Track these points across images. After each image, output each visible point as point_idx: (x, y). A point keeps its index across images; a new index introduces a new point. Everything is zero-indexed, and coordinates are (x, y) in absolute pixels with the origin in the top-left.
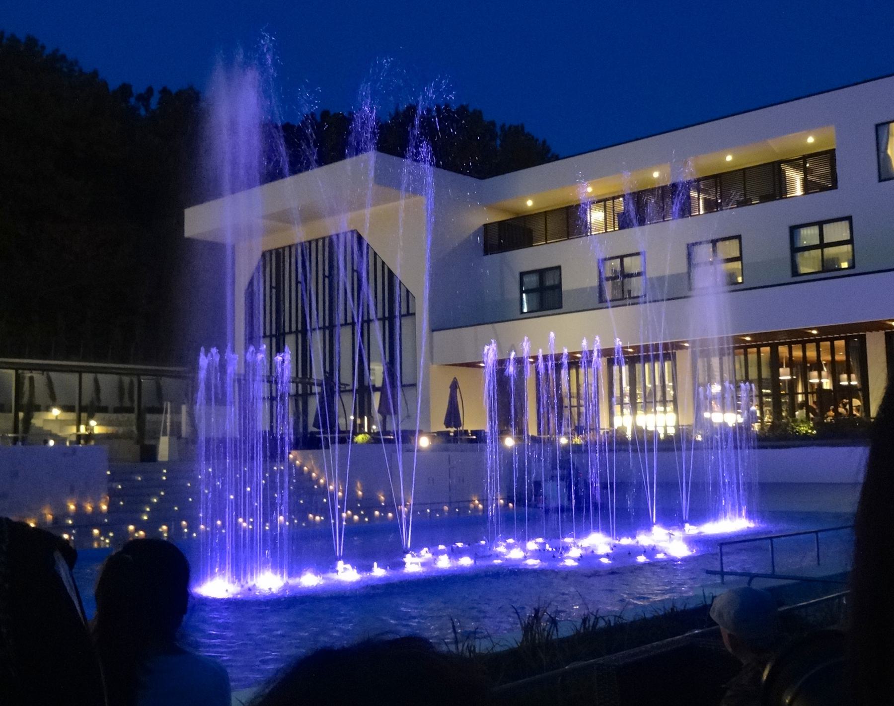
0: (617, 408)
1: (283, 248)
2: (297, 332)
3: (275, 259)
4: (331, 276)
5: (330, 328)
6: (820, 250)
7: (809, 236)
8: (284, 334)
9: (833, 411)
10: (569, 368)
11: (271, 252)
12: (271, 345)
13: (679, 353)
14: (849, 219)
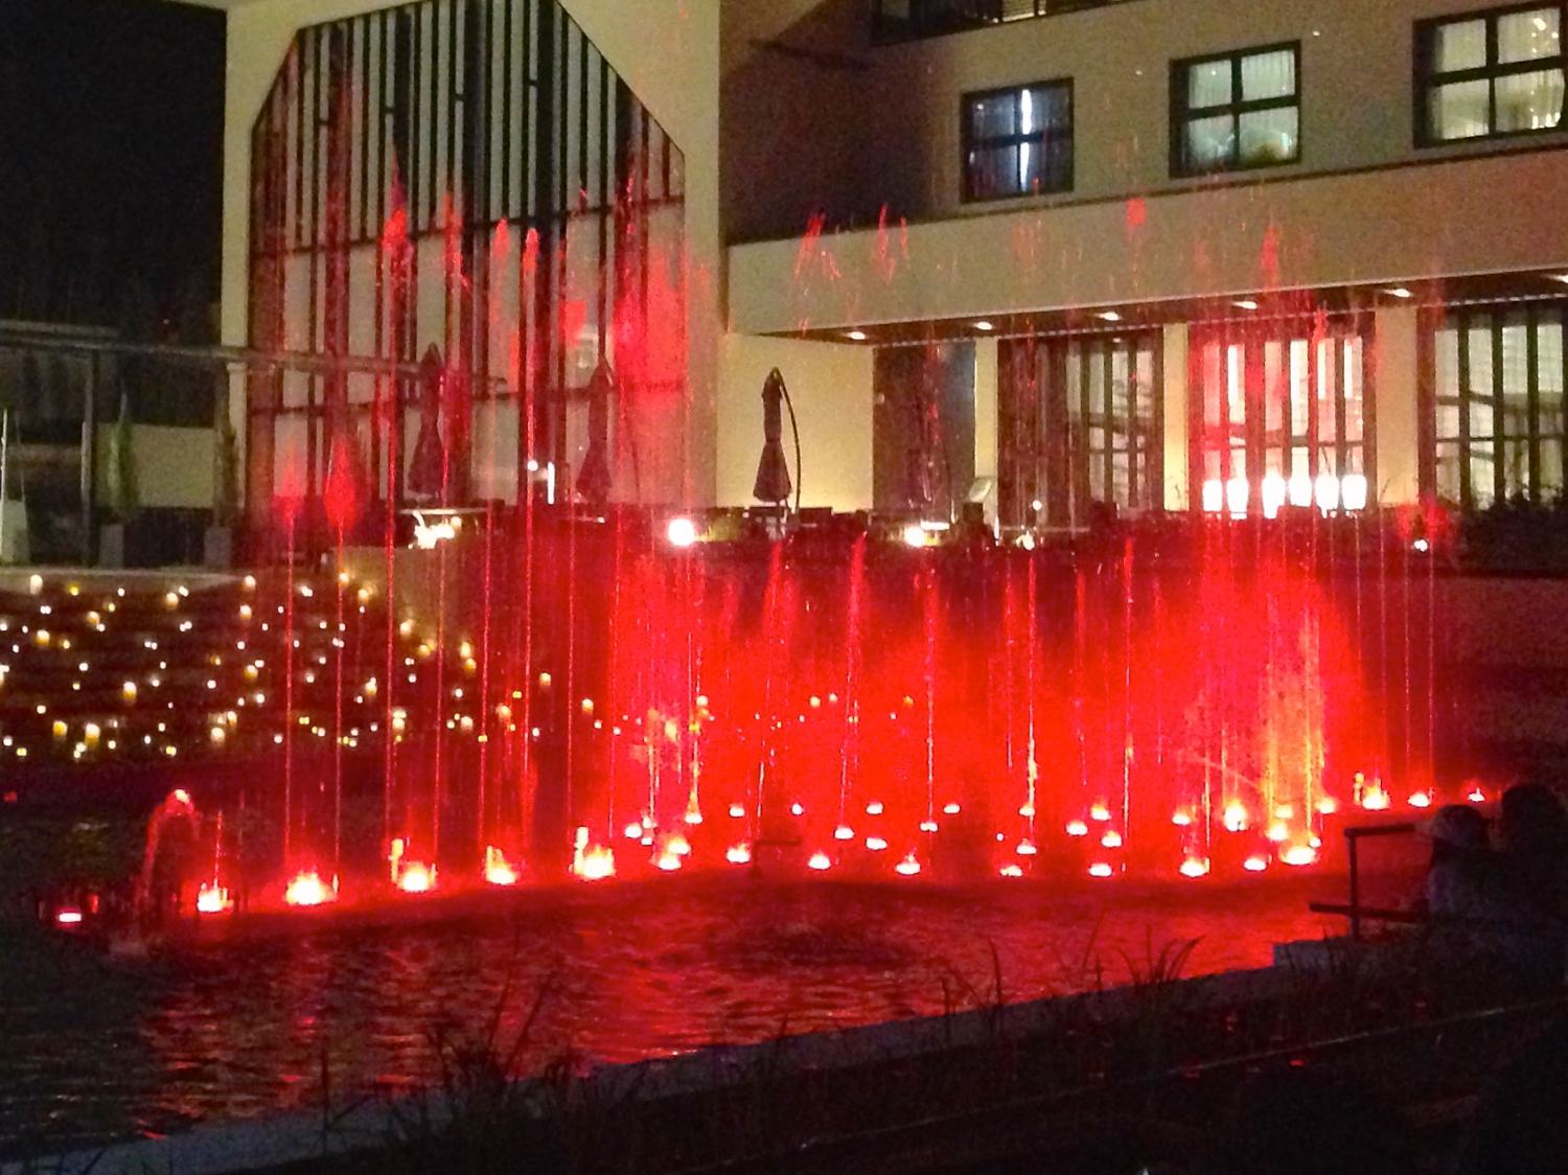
0: (1213, 460)
1: (350, 21)
4: (544, 82)
6: (1487, 82)
7: (1211, 83)
8: (564, 217)
11: (318, 28)
12: (314, 271)
13: (1382, 315)
14: (1295, 46)
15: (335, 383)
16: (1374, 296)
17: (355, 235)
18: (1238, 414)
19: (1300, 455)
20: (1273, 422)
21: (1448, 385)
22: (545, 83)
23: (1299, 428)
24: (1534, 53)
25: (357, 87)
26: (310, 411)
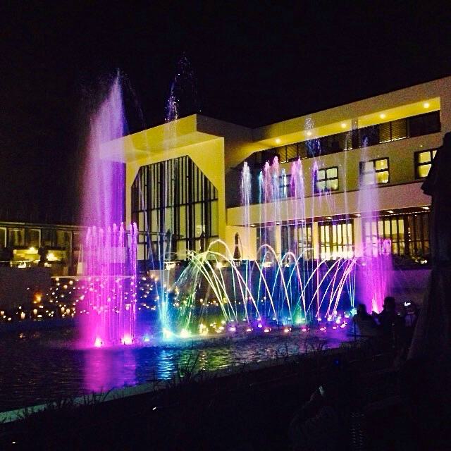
0: (323, 248)
1: (164, 162)
2: (158, 209)
3: (145, 171)
5: (161, 209)
9: (46, 260)
10: (298, 228)
14: (387, 158)
15: (149, 238)
16: (352, 216)
17: (196, 201)
18: (328, 240)
19: (340, 247)
20: (335, 241)
21: (368, 233)
22: (190, 177)
23: (340, 242)
24: (426, 161)
25: (153, 177)
26: (144, 243)
